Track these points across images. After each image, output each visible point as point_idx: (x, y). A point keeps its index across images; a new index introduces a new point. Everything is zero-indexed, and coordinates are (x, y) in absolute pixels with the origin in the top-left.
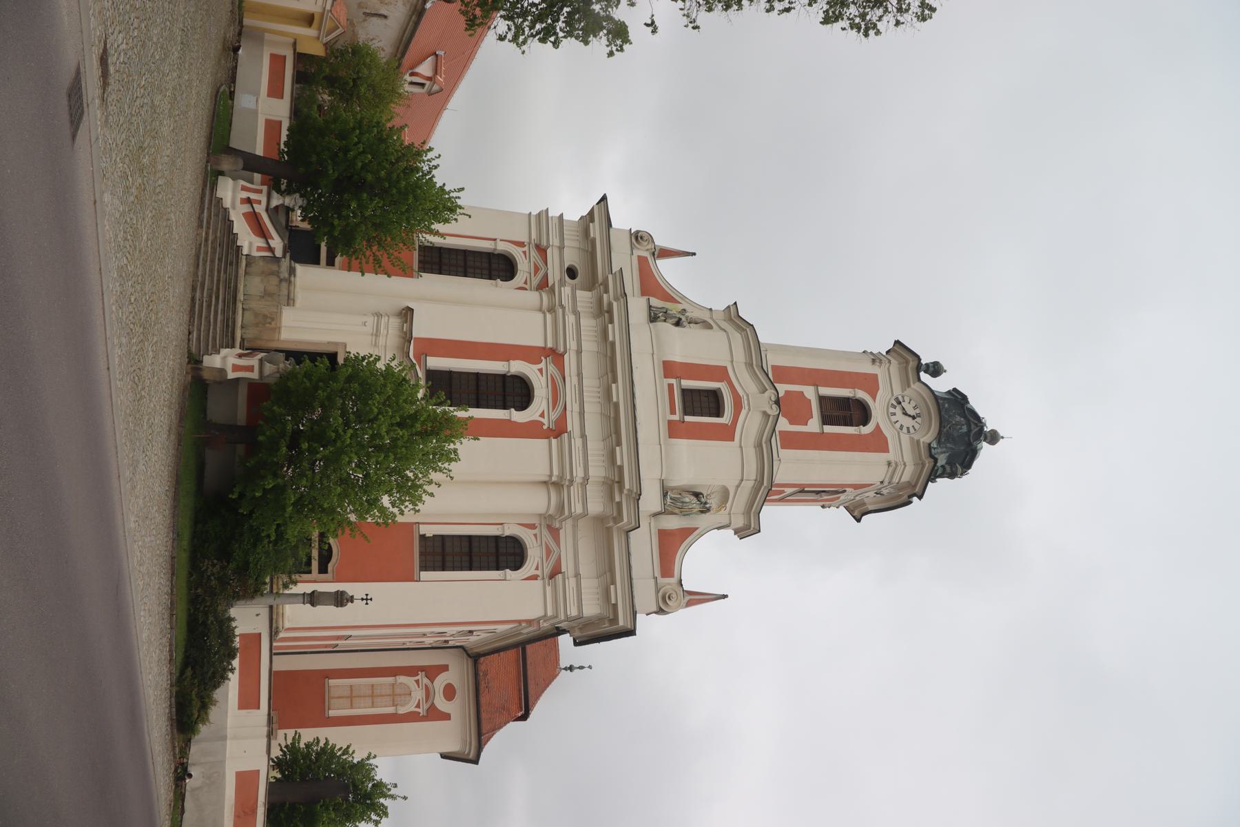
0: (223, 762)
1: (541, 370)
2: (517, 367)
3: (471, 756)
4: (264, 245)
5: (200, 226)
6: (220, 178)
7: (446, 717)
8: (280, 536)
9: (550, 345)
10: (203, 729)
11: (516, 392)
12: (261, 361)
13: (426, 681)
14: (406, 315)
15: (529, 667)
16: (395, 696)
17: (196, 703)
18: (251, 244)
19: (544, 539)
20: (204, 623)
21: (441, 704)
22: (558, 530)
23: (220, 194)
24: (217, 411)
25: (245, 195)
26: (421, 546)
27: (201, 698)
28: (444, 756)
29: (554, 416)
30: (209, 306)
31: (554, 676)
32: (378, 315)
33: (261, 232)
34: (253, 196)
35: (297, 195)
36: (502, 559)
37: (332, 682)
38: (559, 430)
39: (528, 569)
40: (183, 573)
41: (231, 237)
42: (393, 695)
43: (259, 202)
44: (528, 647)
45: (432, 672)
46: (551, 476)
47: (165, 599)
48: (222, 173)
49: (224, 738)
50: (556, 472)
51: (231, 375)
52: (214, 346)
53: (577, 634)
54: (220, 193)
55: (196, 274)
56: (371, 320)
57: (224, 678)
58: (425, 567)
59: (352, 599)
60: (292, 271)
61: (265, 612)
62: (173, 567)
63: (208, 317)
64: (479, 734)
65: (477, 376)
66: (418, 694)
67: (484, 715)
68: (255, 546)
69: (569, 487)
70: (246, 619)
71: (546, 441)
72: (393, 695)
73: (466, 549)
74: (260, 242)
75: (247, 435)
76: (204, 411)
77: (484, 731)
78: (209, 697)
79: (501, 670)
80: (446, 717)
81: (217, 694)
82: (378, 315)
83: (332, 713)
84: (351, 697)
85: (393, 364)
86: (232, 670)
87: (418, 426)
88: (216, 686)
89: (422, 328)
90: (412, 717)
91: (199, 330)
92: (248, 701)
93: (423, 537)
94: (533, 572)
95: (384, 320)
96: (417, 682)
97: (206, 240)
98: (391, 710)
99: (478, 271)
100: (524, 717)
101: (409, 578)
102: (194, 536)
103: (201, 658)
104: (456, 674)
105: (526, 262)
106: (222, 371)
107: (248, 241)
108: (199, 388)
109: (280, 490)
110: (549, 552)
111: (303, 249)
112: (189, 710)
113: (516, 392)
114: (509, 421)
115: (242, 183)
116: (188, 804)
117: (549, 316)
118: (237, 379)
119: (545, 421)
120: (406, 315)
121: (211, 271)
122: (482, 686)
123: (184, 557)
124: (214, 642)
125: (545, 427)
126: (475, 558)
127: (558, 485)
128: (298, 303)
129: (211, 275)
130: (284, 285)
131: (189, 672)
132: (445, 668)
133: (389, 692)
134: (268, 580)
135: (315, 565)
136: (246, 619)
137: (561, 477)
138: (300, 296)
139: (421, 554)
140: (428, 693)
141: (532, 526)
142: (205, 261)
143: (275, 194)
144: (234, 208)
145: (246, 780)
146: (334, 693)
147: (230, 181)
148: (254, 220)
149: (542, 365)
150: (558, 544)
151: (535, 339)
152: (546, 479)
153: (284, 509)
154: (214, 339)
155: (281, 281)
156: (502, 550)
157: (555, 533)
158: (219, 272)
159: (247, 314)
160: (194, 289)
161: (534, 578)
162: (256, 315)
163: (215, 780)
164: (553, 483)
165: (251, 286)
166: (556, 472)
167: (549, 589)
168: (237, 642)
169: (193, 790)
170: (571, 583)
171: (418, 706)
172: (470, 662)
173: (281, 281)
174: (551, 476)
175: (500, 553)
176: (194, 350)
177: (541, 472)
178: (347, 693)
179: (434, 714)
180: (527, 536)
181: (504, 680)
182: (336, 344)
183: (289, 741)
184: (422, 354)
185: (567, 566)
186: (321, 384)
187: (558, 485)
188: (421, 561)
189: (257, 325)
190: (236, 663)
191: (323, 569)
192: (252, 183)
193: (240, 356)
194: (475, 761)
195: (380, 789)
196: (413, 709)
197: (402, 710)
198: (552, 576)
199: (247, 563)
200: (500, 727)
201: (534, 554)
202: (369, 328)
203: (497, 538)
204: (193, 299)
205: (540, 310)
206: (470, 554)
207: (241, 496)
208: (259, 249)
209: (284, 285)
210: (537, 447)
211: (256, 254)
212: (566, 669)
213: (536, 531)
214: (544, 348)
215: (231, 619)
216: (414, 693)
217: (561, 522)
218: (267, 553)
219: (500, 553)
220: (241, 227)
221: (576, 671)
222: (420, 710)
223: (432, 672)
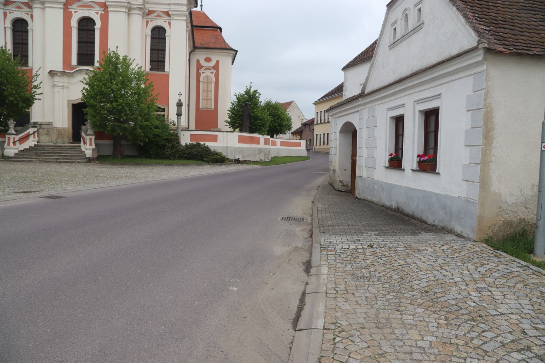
0: (235, 148)
1: (75, 12)
2: (74, 23)
3: (234, 53)
4: (33, 135)
5: (31, 161)
6: (4, 155)
7: (218, 62)
8: (156, 127)
9: (62, 6)
10: (224, 154)
11: (86, 25)
12: (86, 135)
13: (203, 69)
14: (53, 74)
15: (199, 25)
16: (208, 83)
17: (216, 156)
18: (33, 141)
19: (153, 17)
20: (188, 154)
21: (212, 64)
22: (149, 11)
23: (13, 155)
24: (108, 151)
25: (11, 144)
26: (154, 71)
27: (214, 155)
28: (232, 64)
29: (98, 8)
30: (65, 156)
31: (204, 14)
32: (54, 86)
33: (27, 137)
34: (12, 141)
35: (9, 122)
36: (161, 37)
37: (201, 107)
38: (104, 6)
39: (165, 26)
40: (171, 162)
41: (31, 149)
42: (207, 83)
43: (14, 138)
44: (194, 24)
45: (199, 66)
46: (126, 12)
47: (181, 167)
48: (3, 154)
49: (227, 147)
50: (124, 10)
51: (94, 146)
52: (81, 153)
53: (192, 6)
54: (12, 154)
55: (53, 162)
56: (57, 89)
57: (207, 147)
58: (163, 70)
59: (180, 100)
60: (35, 123)
61: (183, 133)
62: (169, 165)
63: (70, 156)
64: (226, 49)
65: (79, 42)
66: (208, 73)
67: (219, 46)
68: (160, 136)
69: (131, 4)
70: (185, 139)
71: (110, 13)
72: (207, 83)
73: (156, 52)
74: (31, 137)
75: (116, 140)
76: (108, 156)
77: (225, 47)
78: (213, 152)
79: (202, 37)
80: (218, 62)
81: (212, 149)
82: (54, 86)
83: (213, 107)
84: (207, 100)
85: (85, 82)
86: (204, 144)
87: (114, 72)
88: (210, 150)
89: (59, 66)
90: (217, 76)
91: (76, 159)
92: (214, 139)
93: (151, 70)
94: (167, 24)
95: (56, 83)
96: (203, 73)
97: (36, 159)
98: (213, 85)
99: (24, 38)
100: (221, 29)
101: (168, 76)
102: (155, 158)
103: (199, 155)
104: (201, 56)
105: (15, 13)
106: (93, 150)
107: (31, 142)
108: (100, 158)
109: (142, 127)
110: (159, 16)
111: (24, 121)
112: (218, 159)
113: (86, 25)
114: (100, 29)
115: (6, 146)
116: (247, 159)
117: (47, 5)
118: (95, 144)
119: (100, 12)
120: (53, 74)
121: (50, 156)
122: (206, 46)
123: (165, 161)
124: (195, 150)
125: (103, 13)
126: (160, 48)
127: (130, 9)
128: (51, 121)
129: (52, 156)
130: (43, 126)
131: (205, 159)
132: (198, 61)
133: (206, 85)
134: (172, 132)
135: (162, 113)
136: (185, 139)
137: (126, 7)
138: (47, 120)
139: (158, 71)
140: (208, 69)
141: (147, 22)
142: (46, 159)
143: (9, 132)
144: (18, 149)
145: (241, 140)
146: (205, 106)
147: (6, 151)
148: (22, 140)
149: (73, 11)
150: (155, 11)
151: (59, 14)
152: (127, 14)
153: (148, 126)
154: (78, 153)
155: (41, 128)
156: (157, 36)
157: (150, 12)
158: (49, 153)
159: (58, 142)
160: (60, 162)
161: (170, 23)
162: (58, 138)
163: (241, 150)
164: (129, 11)
165: (45, 140)
166: (124, 10)
167: (175, 18)
168: (195, 142)
169: (243, 157)
170: (173, 7)
171: (213, 73)
172: (196, 50)
173: (41, 128)
174: (126, 12)
175: (158, 36)
176: (85, 161)
177: (124, 16)
178: (205, 101)
179: (216, 67)
180: (152, 25)
181: (206, 35)
182: (68, 104)
183: (228, 124)
184: (71, 67)
185: (165, 8)
186: (98, 111)
187: (130, 9)
188: (161, 71)
189: (63, 137)
190: (202, 143)
191: (164, 110)
192: (5, 142)
193: (85, 143)
194: (236, 52)
195: (247, 92)
196: (214, 75)
197: (214, 80)
198: (169, 15)
199: (166, 139)
200: (224, 40)
201: (159, 22)
202: (61, 90)
203: (152, 38)
204: (64, 162)
205: (44, 9)
206: (158, 50)
207: (141, 141)
208: (34, 137)
209: (43, 126)
210: (112, 16)
211: (37, 139)
212: (201, 8)
213: (149, 20)
214: (64, 9)
215: (186, 145)
216: (206, 74)
217: (146, 9)
218: (163, 132)
219: (158, 36)
220: (26, 145)
221: (203, 4)
222: (214, 73)
223: (199, 66)
